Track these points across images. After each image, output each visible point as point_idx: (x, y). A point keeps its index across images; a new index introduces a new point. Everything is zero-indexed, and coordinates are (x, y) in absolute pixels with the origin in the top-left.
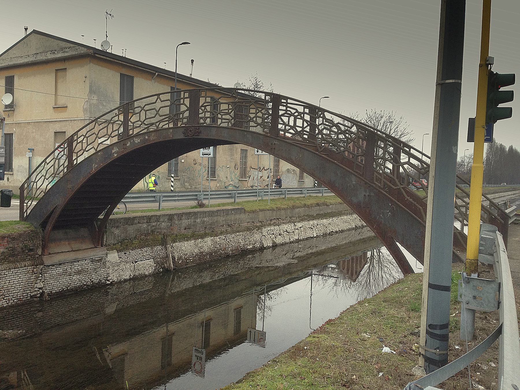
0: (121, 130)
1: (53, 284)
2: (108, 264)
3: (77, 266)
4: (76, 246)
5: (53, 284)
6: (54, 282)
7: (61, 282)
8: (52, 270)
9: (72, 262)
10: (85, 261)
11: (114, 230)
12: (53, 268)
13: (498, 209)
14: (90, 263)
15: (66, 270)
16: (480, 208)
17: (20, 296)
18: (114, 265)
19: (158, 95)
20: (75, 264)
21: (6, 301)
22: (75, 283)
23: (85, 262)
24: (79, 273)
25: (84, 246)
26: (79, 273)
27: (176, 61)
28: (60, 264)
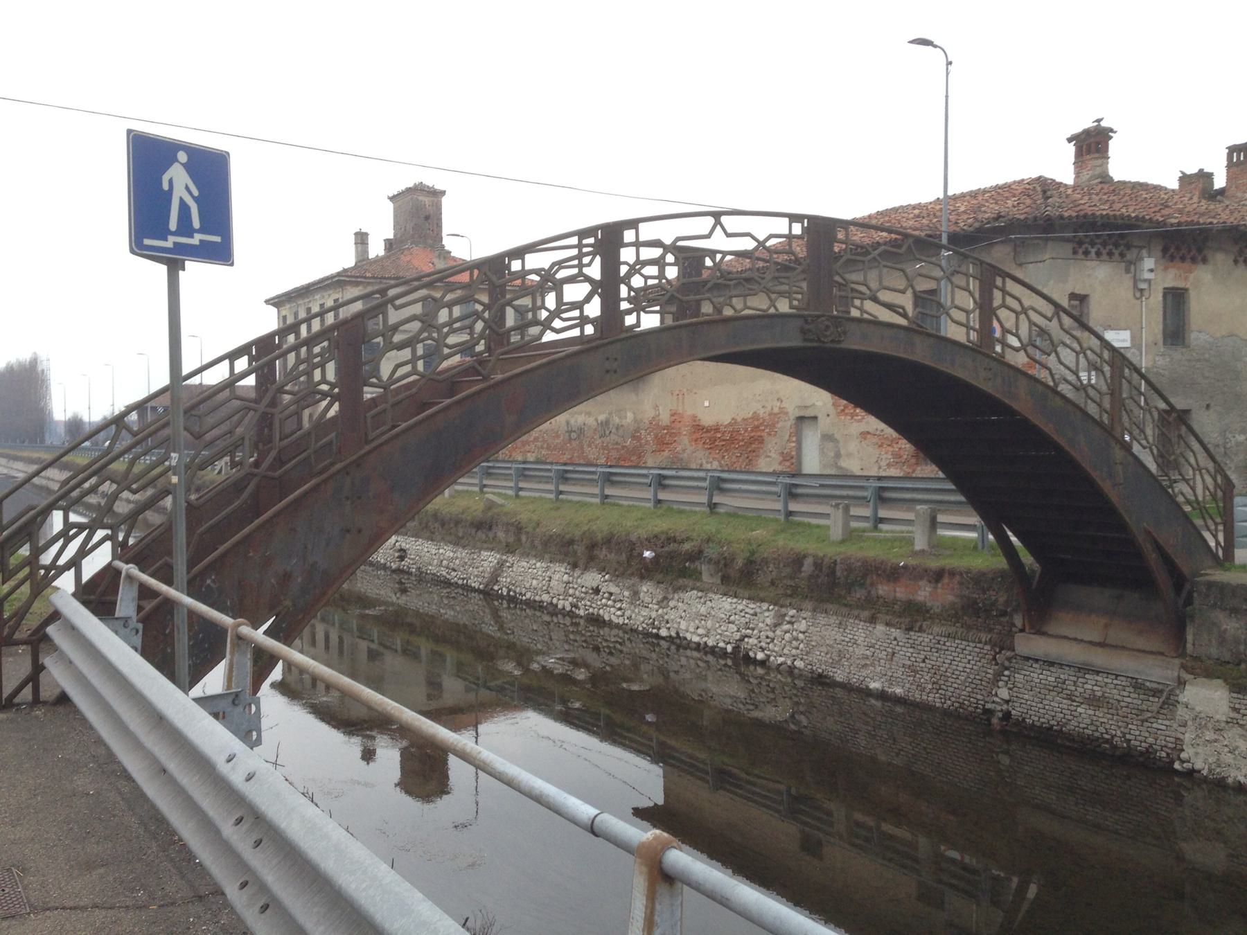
0: (594, 309)
1: (1029, 702)
2: (1181, 712)
3: (1091, 684)
4: (1119, 634)
5: (1029, 702)
6: (1032, 699)
7: (1047, 707)
8: (1032, 669)
9: (1084, 669)
10: (1116, 679)
11: (1220, 616)
12: (1034, 665)
13: (978, 263)
14: (1127, 689)
15: (1064, 683)
16: (193, 703)
17: (964, 700)
18: (1202, 722)
19: (717, 215)
20: (1087, 676)
21: (941, 698)
22: (1081, 725)
23: (1115, 682)
24: (1094, 701)
25: (1140, 643)
26: (1094, 701)
27: (947, 97)
28: (1052, 664)
